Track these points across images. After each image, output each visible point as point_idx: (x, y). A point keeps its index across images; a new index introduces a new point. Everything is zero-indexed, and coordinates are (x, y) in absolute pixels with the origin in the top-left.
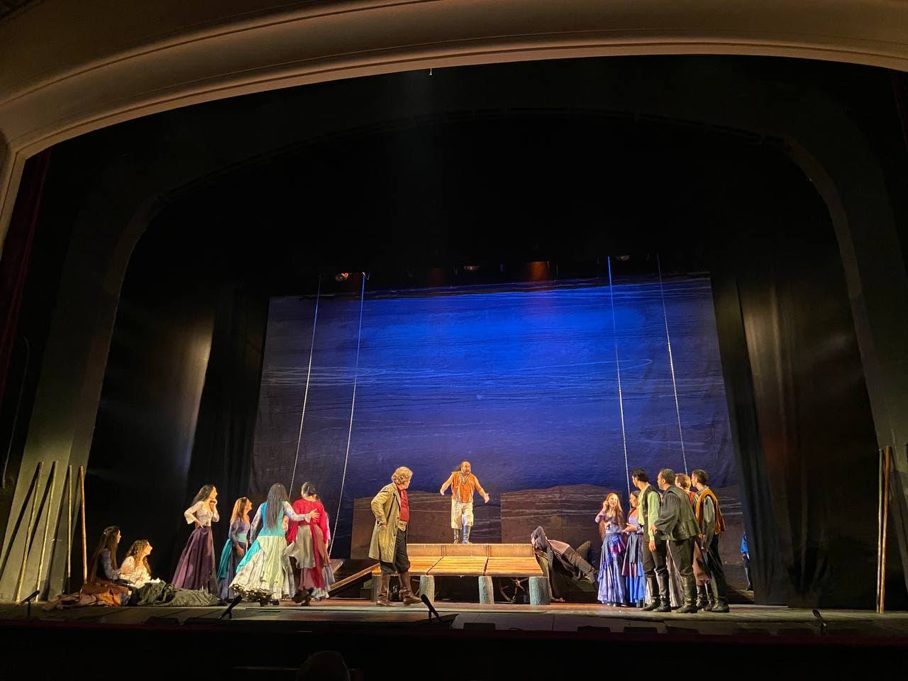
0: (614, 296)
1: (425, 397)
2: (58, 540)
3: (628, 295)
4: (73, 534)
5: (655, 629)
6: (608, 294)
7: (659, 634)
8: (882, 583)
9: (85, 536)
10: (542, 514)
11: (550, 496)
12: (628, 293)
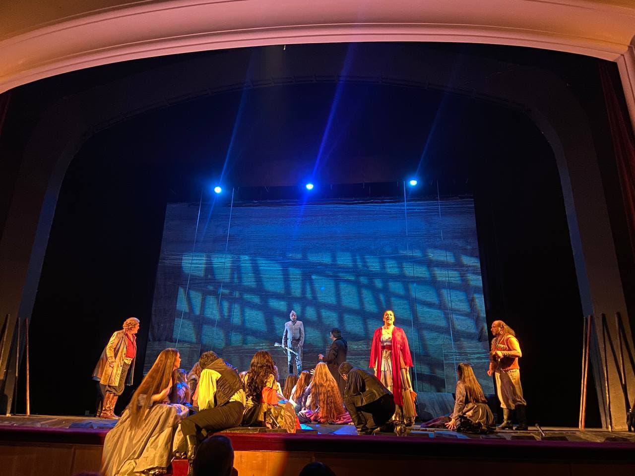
0: (407, 209)
1: (276, 276)
2: (9, 371)
3: (418, 209)
4: (21, 362)
5: (427, 435)
6: (408, 208)
7: (431, 438)
8: (584, 409)
9: (28, 368)
10: (355, 359)
11: (360, 347)
12: (418, 208)
